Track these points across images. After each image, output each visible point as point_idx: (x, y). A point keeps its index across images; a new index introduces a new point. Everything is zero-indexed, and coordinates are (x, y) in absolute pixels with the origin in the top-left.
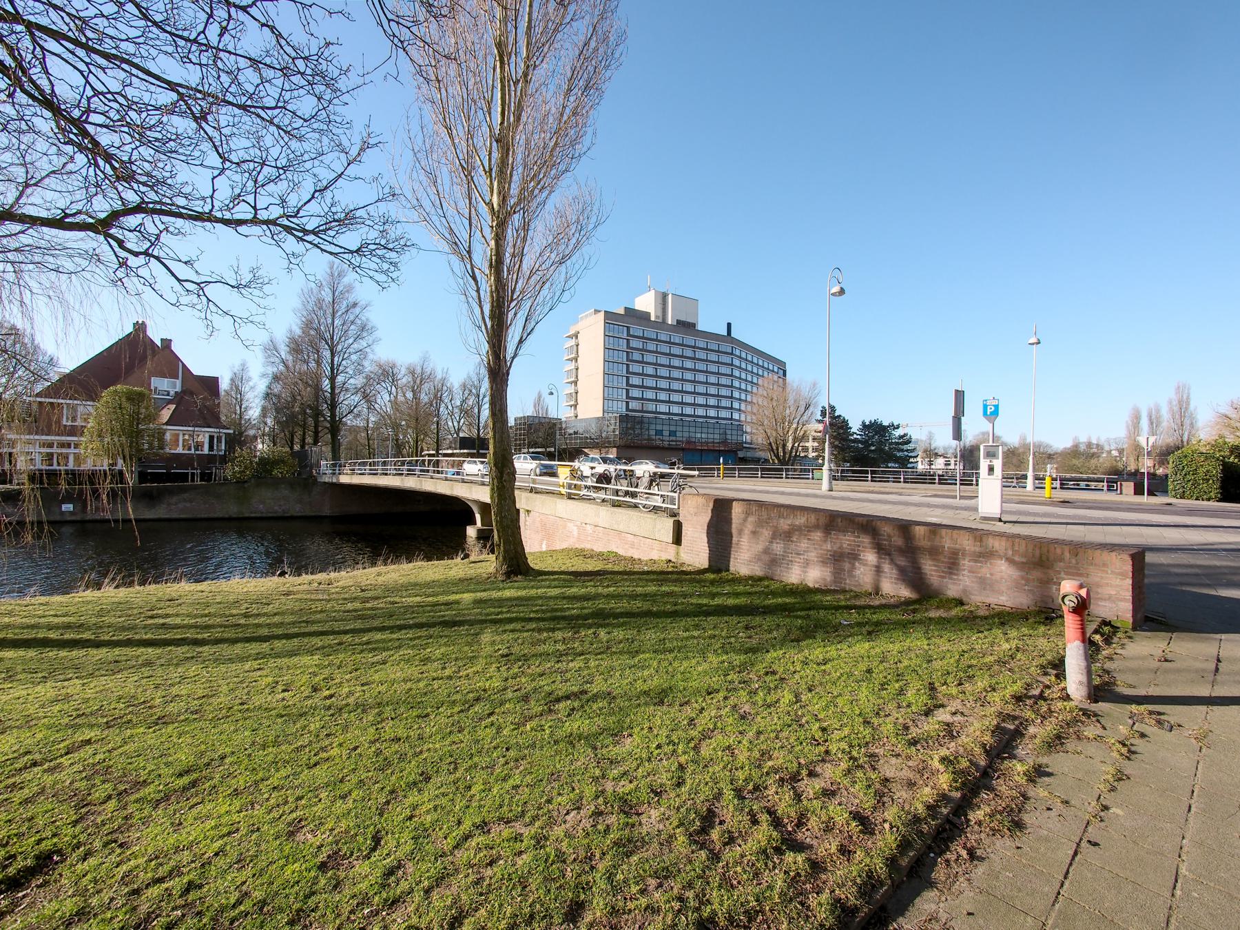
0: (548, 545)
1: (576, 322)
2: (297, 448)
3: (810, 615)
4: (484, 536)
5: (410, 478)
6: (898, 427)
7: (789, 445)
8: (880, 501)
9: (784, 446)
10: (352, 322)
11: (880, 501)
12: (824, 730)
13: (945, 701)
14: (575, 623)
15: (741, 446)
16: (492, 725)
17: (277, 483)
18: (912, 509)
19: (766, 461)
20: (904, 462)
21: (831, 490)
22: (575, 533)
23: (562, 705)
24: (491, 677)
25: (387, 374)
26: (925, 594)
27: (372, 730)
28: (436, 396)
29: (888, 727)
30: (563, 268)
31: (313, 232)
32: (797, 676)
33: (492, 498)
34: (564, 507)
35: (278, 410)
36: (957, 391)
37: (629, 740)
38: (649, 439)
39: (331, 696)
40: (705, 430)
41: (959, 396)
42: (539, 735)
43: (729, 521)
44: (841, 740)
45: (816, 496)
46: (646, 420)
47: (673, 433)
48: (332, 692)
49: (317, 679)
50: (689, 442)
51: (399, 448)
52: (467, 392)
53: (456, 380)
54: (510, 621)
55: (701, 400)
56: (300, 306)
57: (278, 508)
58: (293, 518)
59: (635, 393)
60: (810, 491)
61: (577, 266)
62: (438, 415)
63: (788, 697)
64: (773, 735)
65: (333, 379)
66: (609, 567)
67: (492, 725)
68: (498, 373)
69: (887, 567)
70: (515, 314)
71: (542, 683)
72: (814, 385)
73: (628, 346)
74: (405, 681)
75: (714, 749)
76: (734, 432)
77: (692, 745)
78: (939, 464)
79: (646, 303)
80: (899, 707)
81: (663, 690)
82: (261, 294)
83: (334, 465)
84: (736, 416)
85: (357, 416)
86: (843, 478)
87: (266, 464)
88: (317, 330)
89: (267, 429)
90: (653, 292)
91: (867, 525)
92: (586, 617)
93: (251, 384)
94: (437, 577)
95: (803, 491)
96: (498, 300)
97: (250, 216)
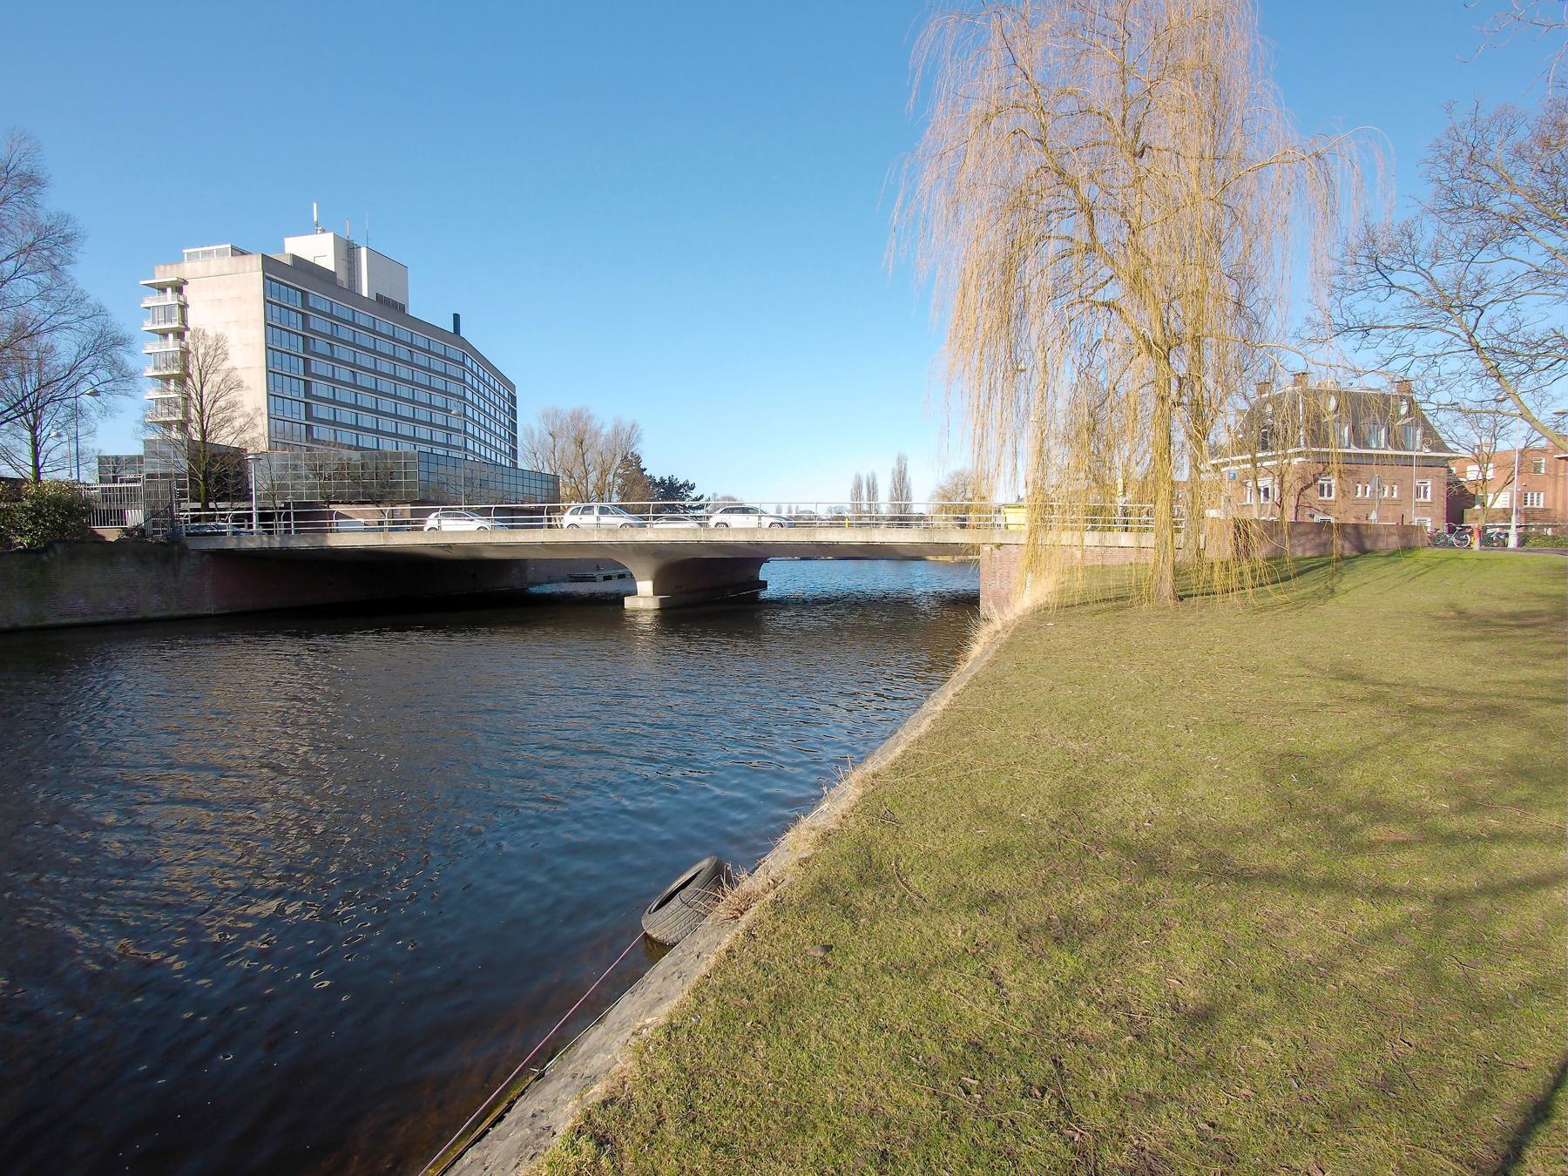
79: (319, 249)
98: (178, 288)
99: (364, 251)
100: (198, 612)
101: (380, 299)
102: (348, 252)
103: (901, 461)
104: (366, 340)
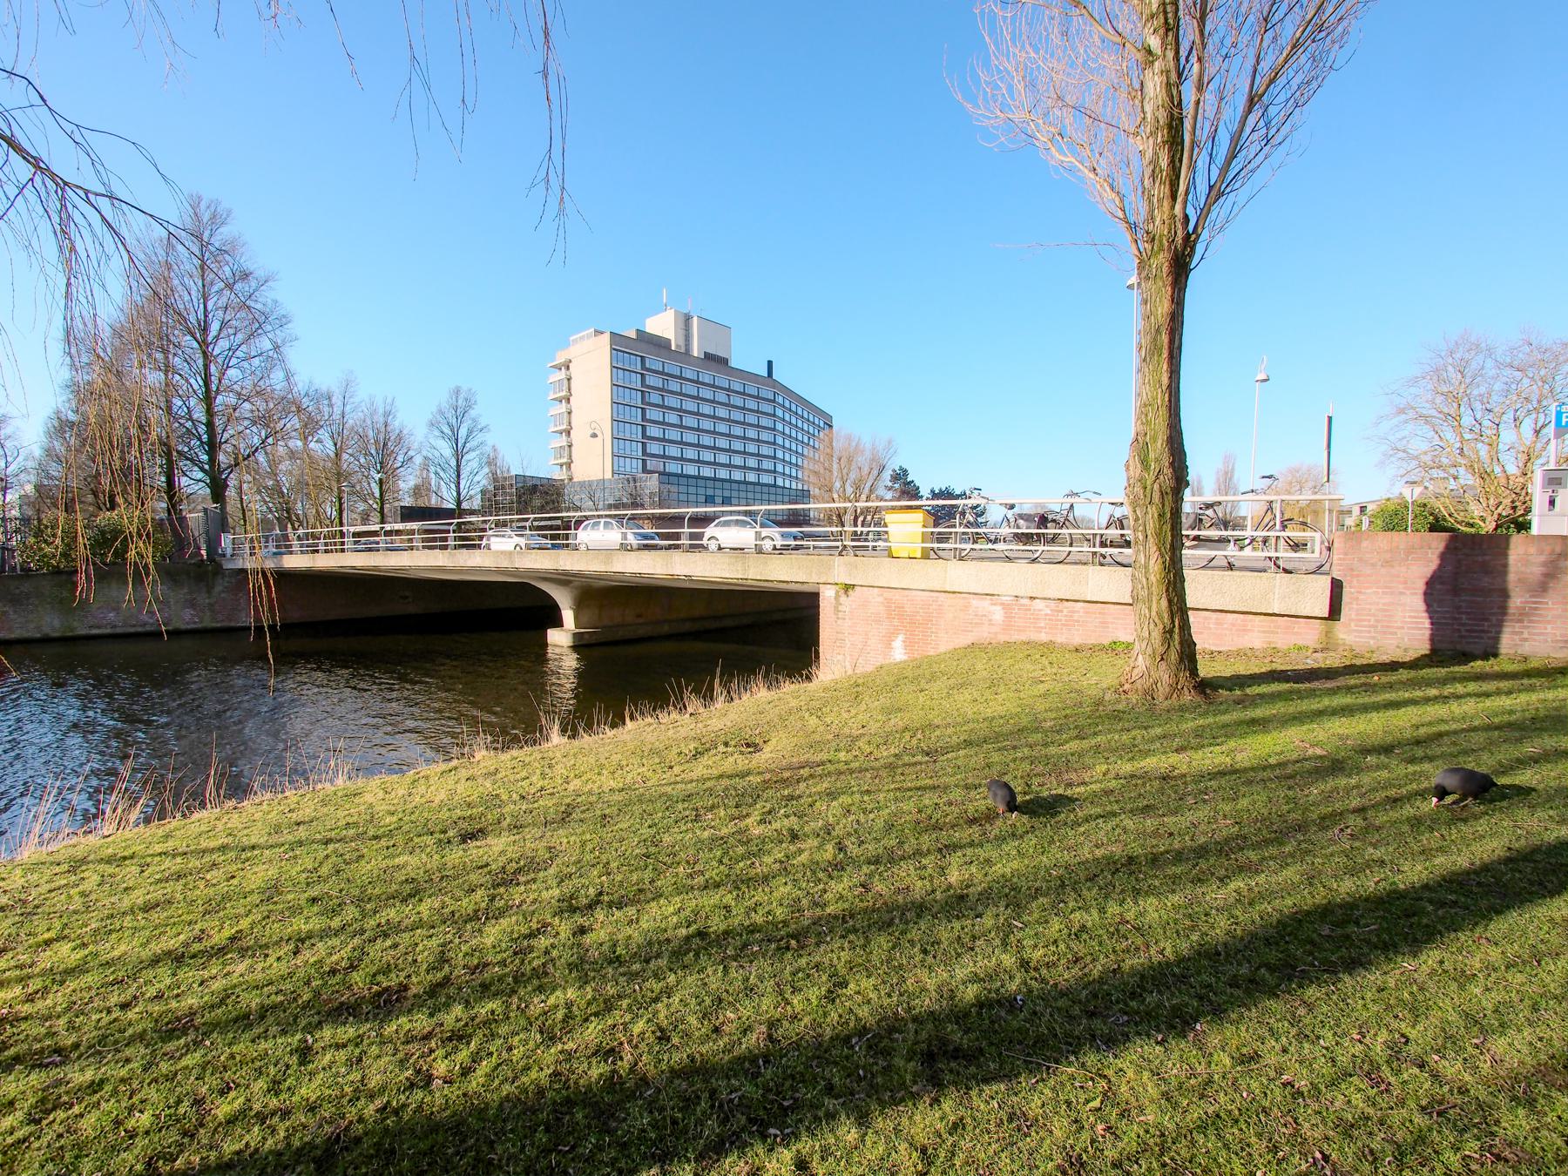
0: (908, 644)
41: (1330, 419)
72: (890, 442)
79: (663, 325)
100: (233, 624)
103: (1229, 459)
104: (690, 389)
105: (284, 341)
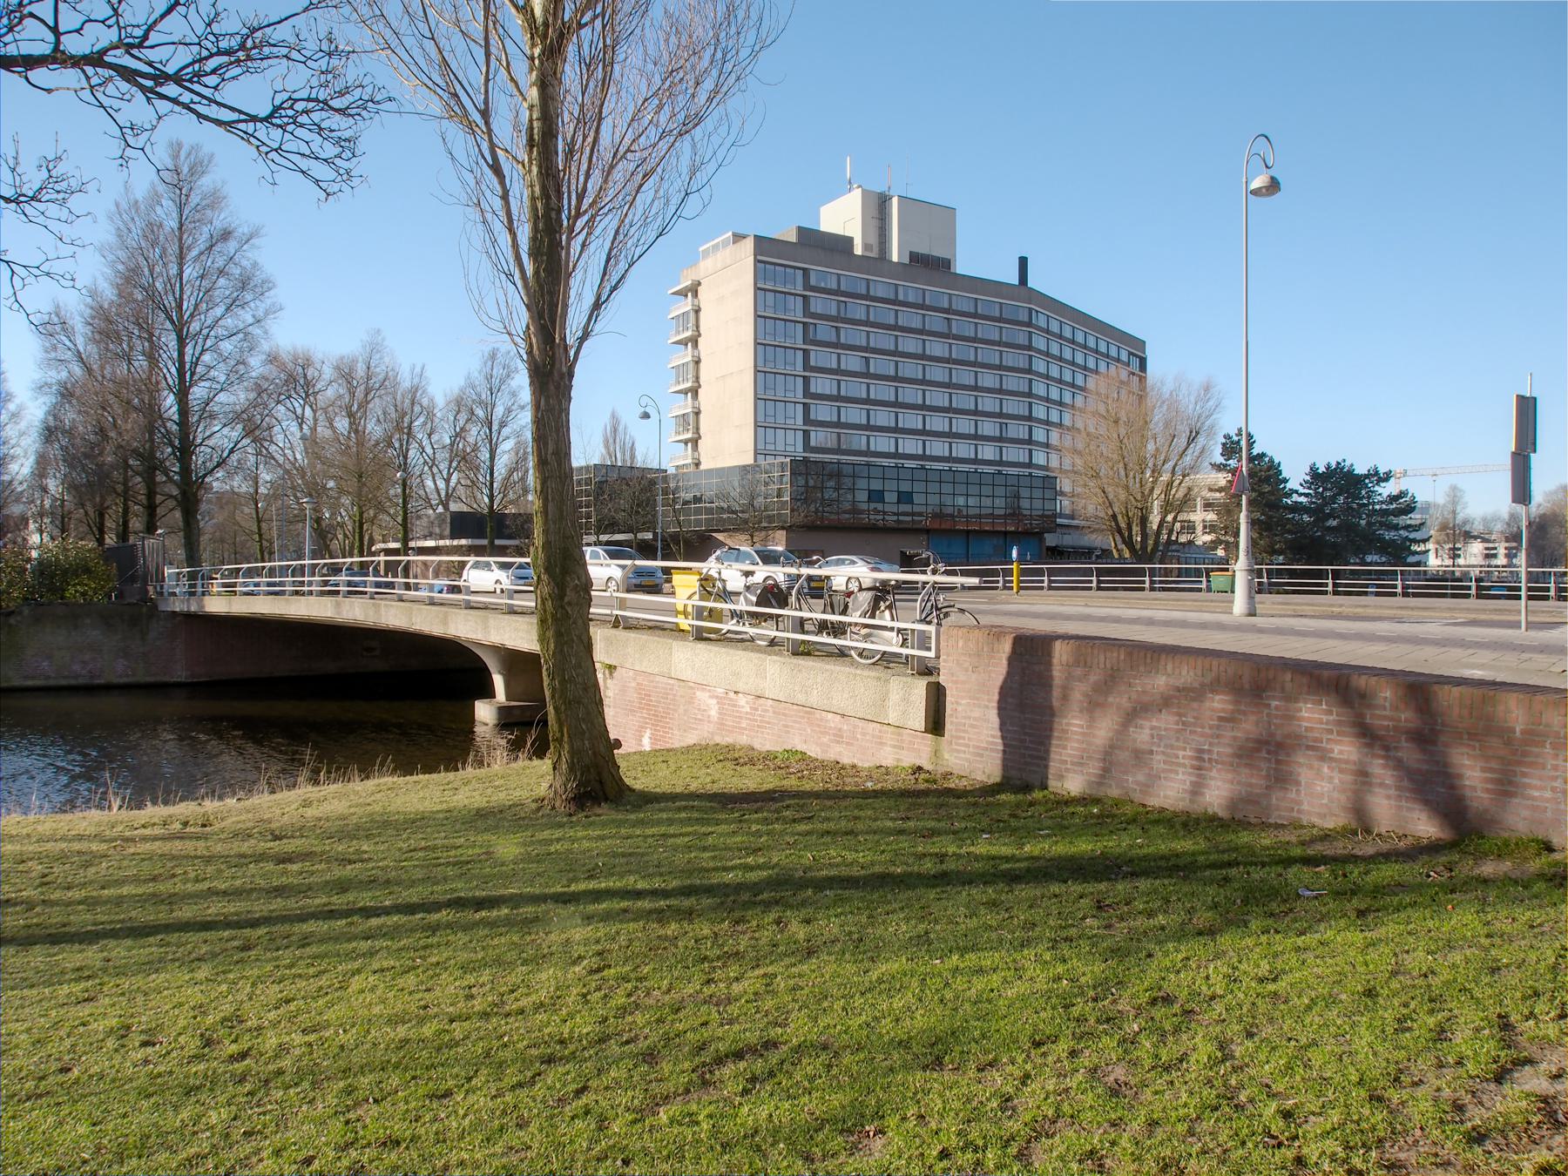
0: (653, 739)
1: (695, 263)
2: (110, 540)
3: (1236, 874)
4: (508, 721)
5: (357, 602)
6: (1387, 477)
7: (1155, 520)
8: (1360, 637)
9: (1144, 521)
10: (221, 272)
11: (1360, 637)
12: (1287, 1115)
13: (1532, 1050)
14: (738, 900)
15: (1050, 522)
16: (587, 1113)
17: (74, 616)
18: (1429, 652)
19: (1105, 554)
20: (1399, 552)
21: (1252, 614)
22: (714, 713)
23: (728, 1070)
24: (571, 1016)
25: (295, 380)
26: (1465, 830)
27: (338, 1124)
28: (399, 428)
29: (1420, 1107)
30: (685, 145)
31: (177, 79)
32: (1219, 1007)
33: (542, 639)
34: (688, 659)
35: (71, 460)
36: (1522, 400)
37: (879, 1142)
38: (855, 511)
39: (243, 1055)
40: (973, 490)
41: (1527, 409)
42: (688, 1133)
43: (1045, 682)
44: (1326, 1134)
45: (1221, 627)
46: (847, 470)
47: (905, 497)
48: (244, 1044)
49: (210, 1020)
50: (939, 516)
51: (323, 540)
52: (463, 417)
53: (441, 388)
54: (597, 896)
55: (964, 425)
56: (112, 238)
57: (79, 670)
58: (109, 688)
59: (823, 412)
60: (1207, 617)
61: (715, 140)
62: (404, 467)
63: (1203, 1050)
64: (1182, 1128)
65: (182, 394)
66: (791, 783)
67: (587, 1113)
68: (552, 374)
69: (1380, 769)
70: (584, 245)
71: (680, 1026)
72: (1207, 389)
73: (806, 311)
74: (394, 1021)
75: (1061, 1158)
76: (1037, 493)
77: (1013, 1150)
78: (1474, 553)
79: (843, 217)
80: (1440, 1066)
81: (939, 1040)
82: (64, 214)
83: (192, 576)
84: (1040, 458)
85: (234, 474)
86: (1274, 589)
87: (51, 576)
88: (150, 292)
89: (47, 503)
90: (857, 193)
91: (1337, 684)
92: (756, 888)
93: (12, 407)
94: (430, 805)
95: (1193, 616)
96: (547, 215)
97: (46, 49)
98: (694, 290)
99: (895, 201)
100: (166, 679)
101: (916, 258)
102: (878, 207)
105: (267, 313)
